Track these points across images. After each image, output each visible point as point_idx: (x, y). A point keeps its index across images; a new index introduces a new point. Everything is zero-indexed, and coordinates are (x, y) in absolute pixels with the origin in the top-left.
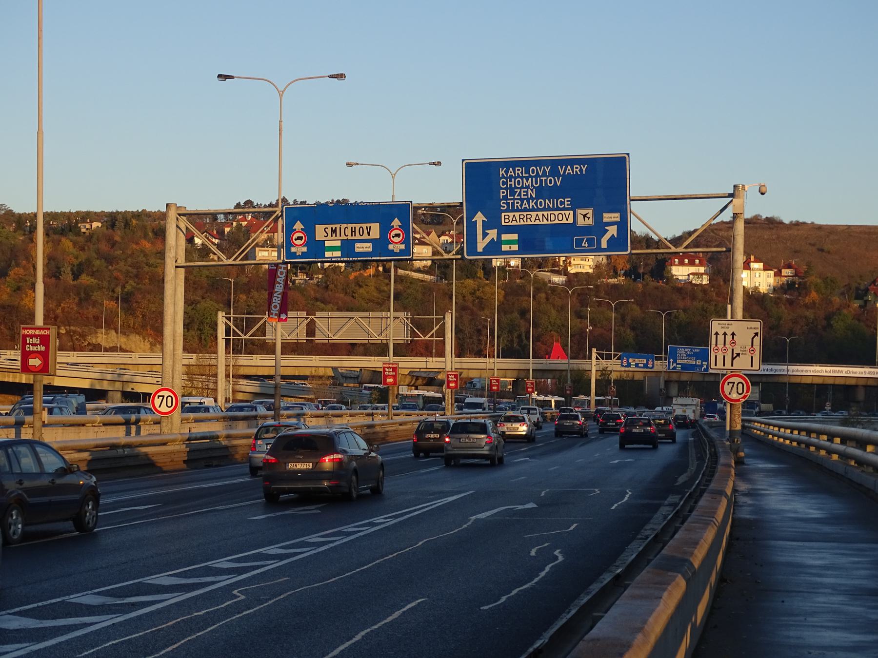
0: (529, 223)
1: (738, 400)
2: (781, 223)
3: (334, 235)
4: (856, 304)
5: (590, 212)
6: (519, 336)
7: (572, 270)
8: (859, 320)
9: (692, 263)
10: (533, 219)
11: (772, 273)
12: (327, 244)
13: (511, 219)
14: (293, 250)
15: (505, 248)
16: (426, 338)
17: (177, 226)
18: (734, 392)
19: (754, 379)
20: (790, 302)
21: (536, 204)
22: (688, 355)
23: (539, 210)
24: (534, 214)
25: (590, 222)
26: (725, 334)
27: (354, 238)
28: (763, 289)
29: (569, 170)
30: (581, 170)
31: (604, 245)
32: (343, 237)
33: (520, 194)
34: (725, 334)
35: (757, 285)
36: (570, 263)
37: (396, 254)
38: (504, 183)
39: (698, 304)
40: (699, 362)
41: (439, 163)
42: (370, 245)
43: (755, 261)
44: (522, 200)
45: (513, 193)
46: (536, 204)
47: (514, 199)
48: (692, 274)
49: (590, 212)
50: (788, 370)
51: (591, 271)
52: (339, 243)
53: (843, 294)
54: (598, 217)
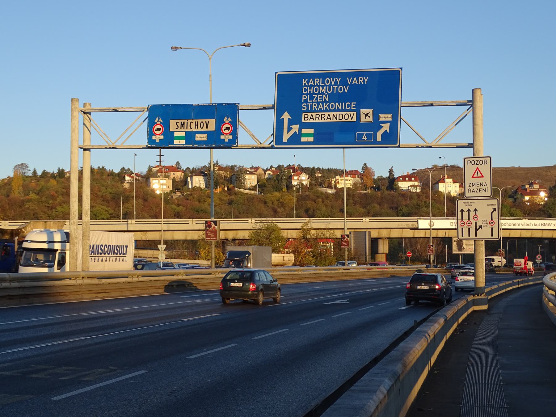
0: (323, 120)
3: (182, 128)
5: (371, 112)
7: (339, 186)
9: (410, 180)
10: (326, 118)
11: (458, 184)
12: (176, 134)
13: (309, 118)
14: (154, 138)
15: (303, 139)
17: (84, 124)
21: (329, 106)
23: (330, 111)
24: (327, 114)
25: (370, 120)
26: (469, 211)
27: (196, 130)
29: (355, 81)
30: (364, 81)
31: (379, 139)
33: (317, 99)
35: (449, 191)
36: (338, 182)
38: (305, 90)
39: (415, 201)
41: (249, 45)
42: (206, 135)
44: (318, 103)
45: (312, 98)
46: (329, 106)
47: (313, 102)
48: (411, 186)
49: (371, 112)
51: (351, 187)
52: (183, 134)
54: (376, 116)
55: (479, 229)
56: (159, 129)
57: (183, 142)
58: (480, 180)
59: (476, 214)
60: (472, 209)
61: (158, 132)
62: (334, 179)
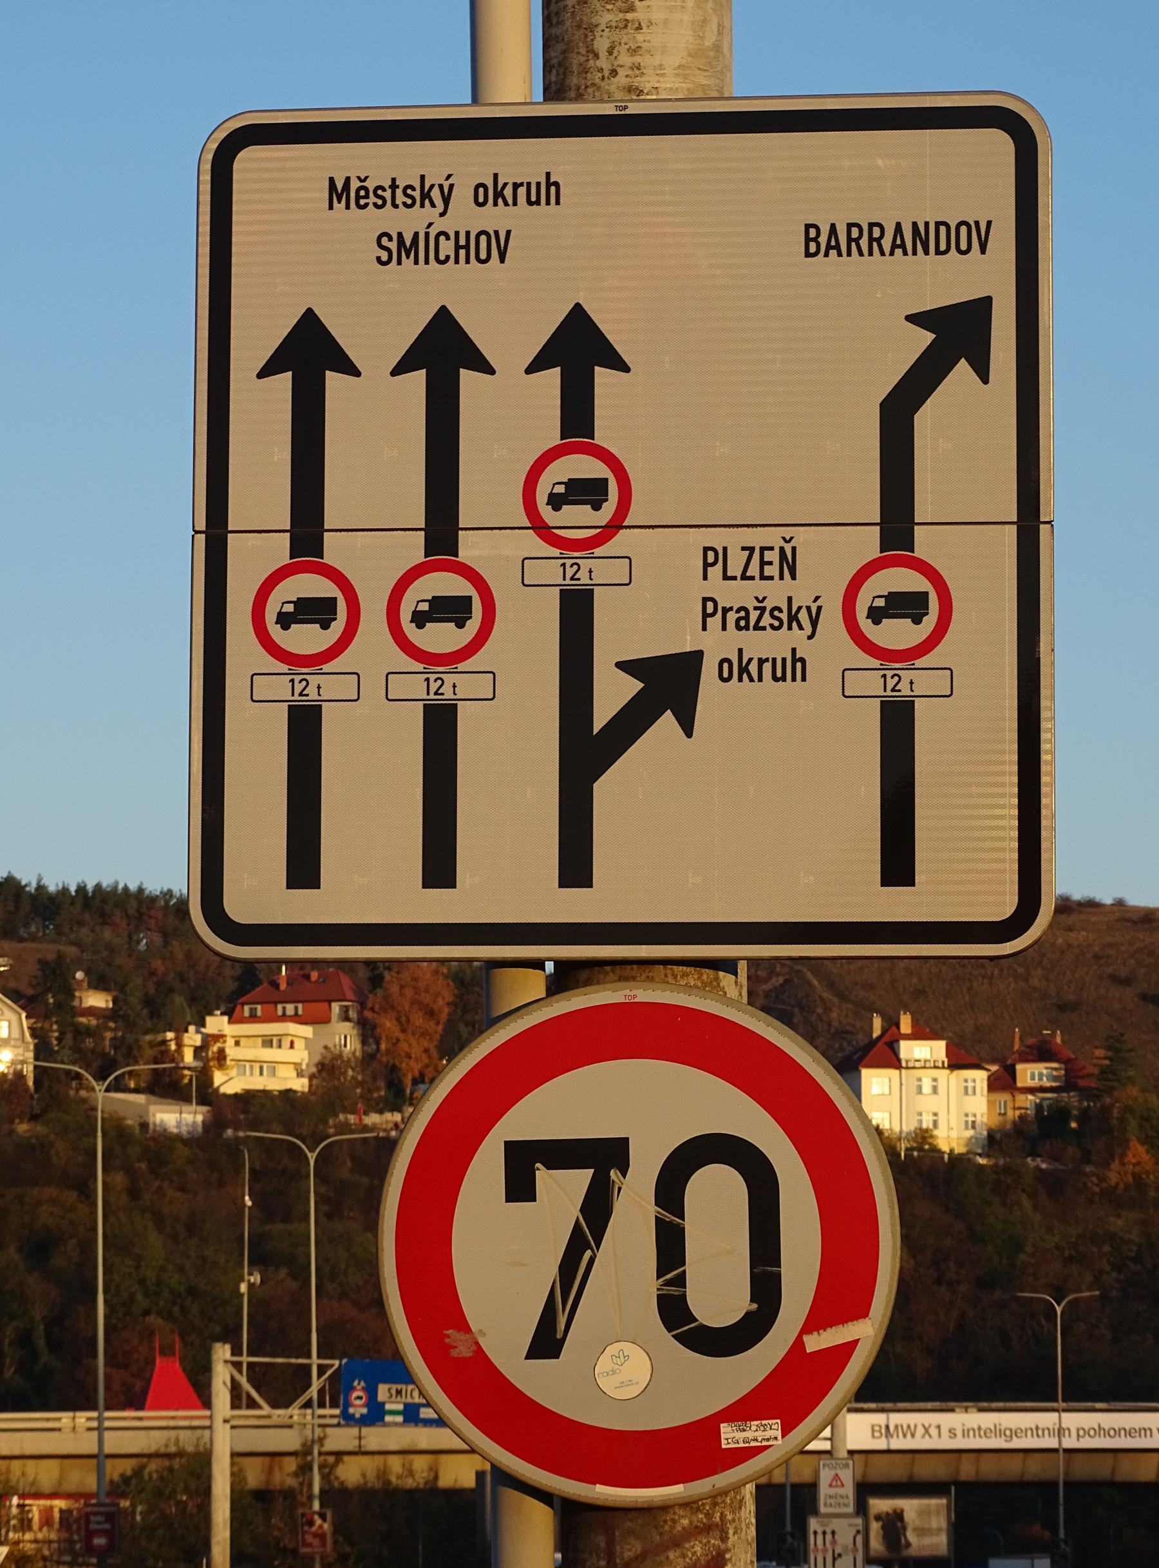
1: (689, 1449)
6: (24, 1339)
7: (229, 1083)
11: (979, 1077)
12: (388, 1407)
14: (351, 1410)
20: (1052, 1184)
28: (951, 1137)
32: (409, 1400)
34: (443, 352)
35: (927, 1122)
36: (221, 1056)
43: (918, 1035)
50: (1061, 1432)
51: (300, 1085)
55: (632, 723)
56: (360, 1398)
57: (400, 1419)
58: (840, 1491)
59: (577, 416)
60: (508, 318)
61: (358, 1402)
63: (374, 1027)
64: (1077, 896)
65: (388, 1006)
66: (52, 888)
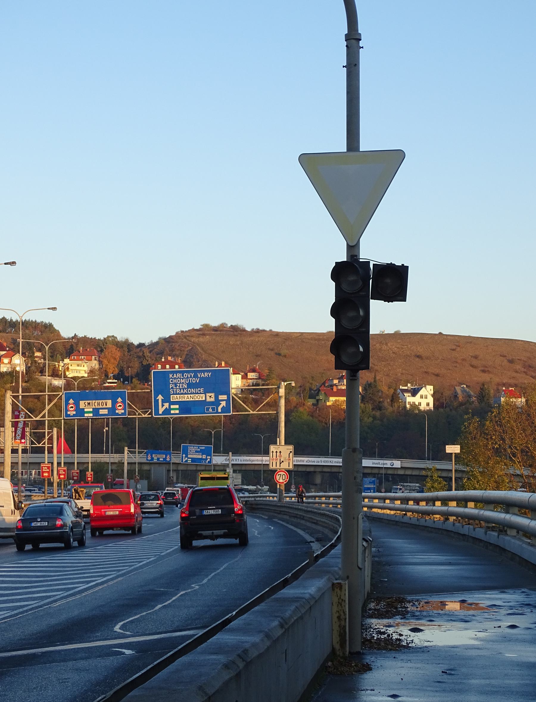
0: (184, 400)
1: (283, 483)
2: (244, 330)
4: (310, 402)
5: (213, 395)
7: (70, 374)
8: (312, 416)
11: (239, 376)
12: (86, 410)
14: (69, 413)
16: (40, 445)
18: (281, 479)
19: (236, 468)
22: (196, 452)
23: (188, 394)
24: (186, 396)
25: (213, 399)
29: (203, 375)
30: (208, 375)
31: (220, 410)
32: (94, 407)
33: (179, 386)
34: (276, 452)
36: (68, 368)
37: (120, 415)
38: (171, 381)
40: (204, 457)
44: (180, 389)
45: (176, 386)
49: (213, 395)
50: (262, 461)
51: (86, 375)
52: (91, 410)
53: (298, 394)
54: (216, 397)
60: (278, 451)
62: (61, 364)
63: (102, 362)
64: (261, 329)
65: (105, 357)
66: (14, 320)
